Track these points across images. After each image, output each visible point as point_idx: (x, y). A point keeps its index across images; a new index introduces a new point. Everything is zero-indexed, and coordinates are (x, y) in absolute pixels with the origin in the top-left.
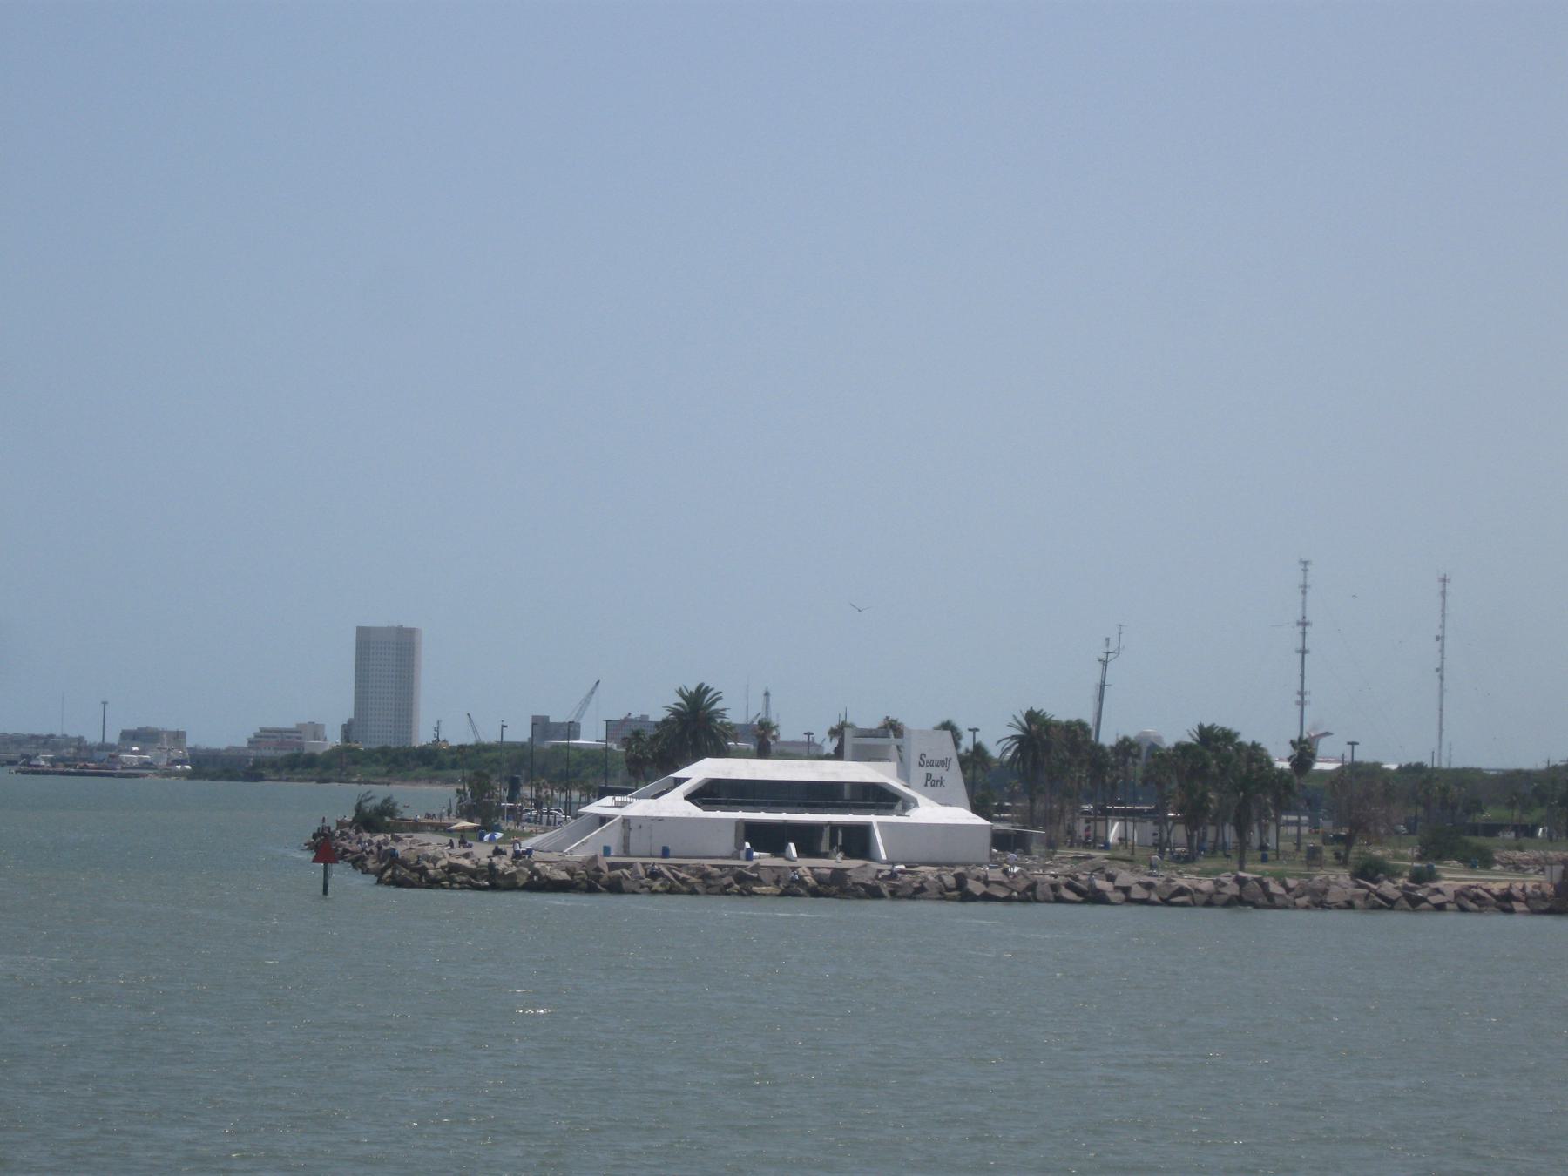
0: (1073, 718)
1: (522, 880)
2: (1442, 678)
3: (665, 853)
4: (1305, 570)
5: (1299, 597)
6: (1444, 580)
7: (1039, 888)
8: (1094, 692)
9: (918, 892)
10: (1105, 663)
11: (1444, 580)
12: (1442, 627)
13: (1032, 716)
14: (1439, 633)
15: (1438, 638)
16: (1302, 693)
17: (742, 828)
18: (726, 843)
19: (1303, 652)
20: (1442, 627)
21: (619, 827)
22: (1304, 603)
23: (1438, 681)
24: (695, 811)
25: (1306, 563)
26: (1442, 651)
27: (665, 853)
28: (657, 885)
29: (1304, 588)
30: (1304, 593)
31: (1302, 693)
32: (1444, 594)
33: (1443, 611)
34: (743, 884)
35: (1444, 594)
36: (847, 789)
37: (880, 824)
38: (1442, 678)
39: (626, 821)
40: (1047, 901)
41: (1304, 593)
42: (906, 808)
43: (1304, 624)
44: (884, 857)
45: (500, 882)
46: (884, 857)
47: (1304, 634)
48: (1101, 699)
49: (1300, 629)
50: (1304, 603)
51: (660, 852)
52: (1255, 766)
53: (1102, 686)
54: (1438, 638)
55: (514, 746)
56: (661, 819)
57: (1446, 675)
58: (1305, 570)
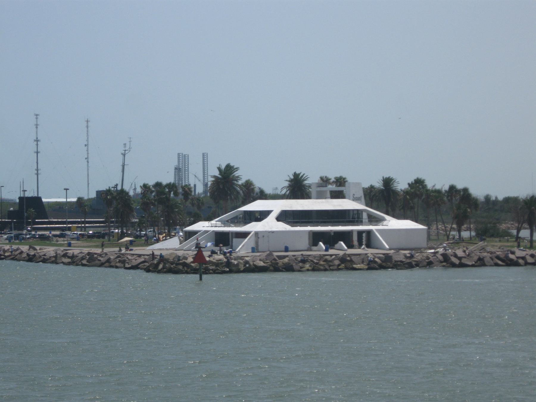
0: (387, 176)
1: (242, 268)
2: (88, 162)
3: (286, 249)
4: (37, 118)
5: (86, 129)
6: (87, 121)
7: (486, 260)
8: (121, 168)
9: (429, 264)
10: (124, 155)
11: (87, 121)
12: (88, 140)
13: (296, 175)
14: (86, 143)
15: (86, 145)
16: (37, 170)
17: (311, 235)
18: (305, 242)
19: (37, 153)
20: (88, 140)
21: (253, 238)
22: (37, 132)
23: (86, 163)
24: (282, 227)
25: (37, 115)
26: (87, 150)
27: (286, 249)
28: (307, 266)
29: (37, 126)
30: (37, 128)
31: (37, 170)
32: (87, 127)
33: (87, 134)
34: (319, 266)
35: (87, 127)
36: (351, 214)
37: (377, 230)
38: (88, 162)
39: (257, 234)
40: (491, 266)
41: (37, 128)
42: (385, 223)
43: (37, 141)
44: (387, 247)
45: (234, 268)
46: (387, 247)
47: (37, 145)
48: (123, 171)
49: (36, 143)
50: (37, 132)
51: (283, 249)
52: (450, 198)
53: (123, 166)
54: (86, 145)
55: (92, 199)
56: (273, 232)
57: (90, 161)
58: (37, 118)
